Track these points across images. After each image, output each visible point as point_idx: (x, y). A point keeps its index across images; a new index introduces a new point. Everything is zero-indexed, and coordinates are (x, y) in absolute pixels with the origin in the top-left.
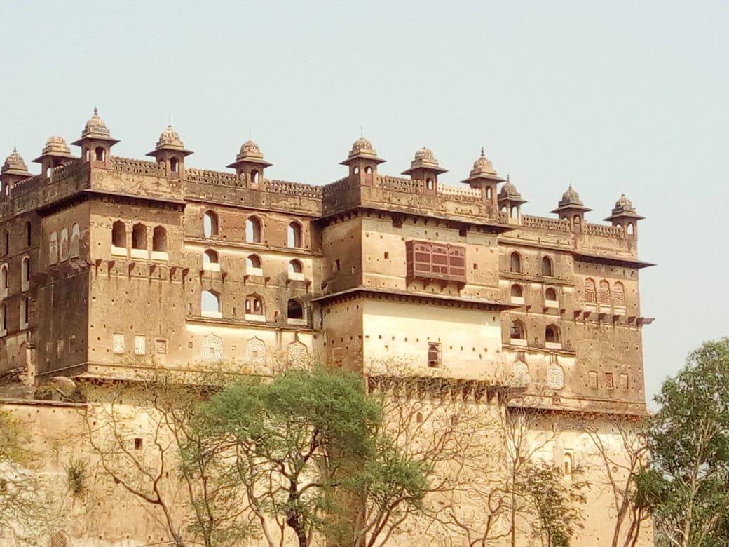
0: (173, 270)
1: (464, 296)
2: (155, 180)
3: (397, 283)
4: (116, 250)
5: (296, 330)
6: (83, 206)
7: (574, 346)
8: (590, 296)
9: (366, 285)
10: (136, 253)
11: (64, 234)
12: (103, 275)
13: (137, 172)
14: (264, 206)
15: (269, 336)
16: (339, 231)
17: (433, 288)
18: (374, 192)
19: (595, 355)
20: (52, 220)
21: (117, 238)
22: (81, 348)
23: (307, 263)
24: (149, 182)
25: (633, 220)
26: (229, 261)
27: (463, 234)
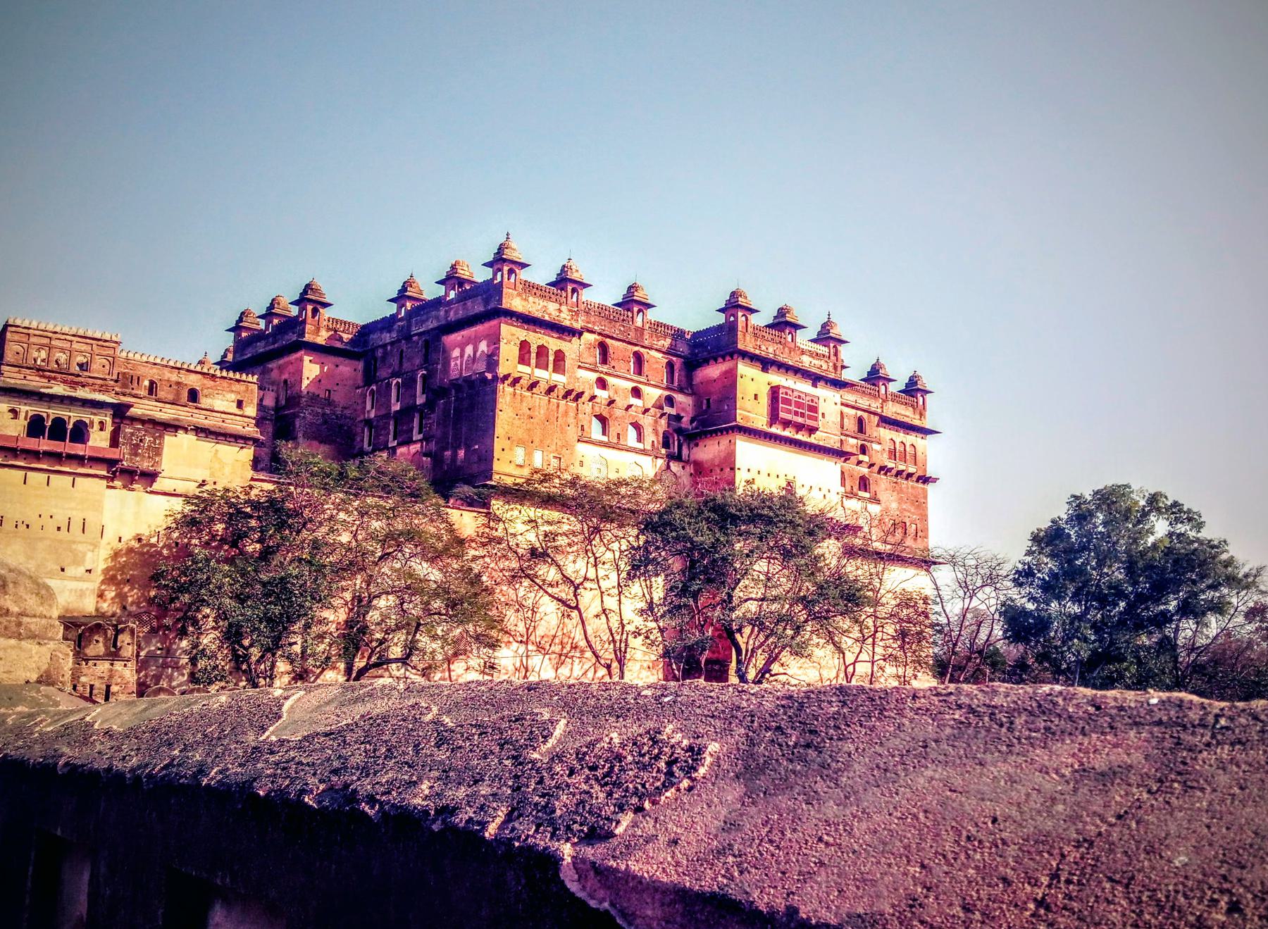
2: (557, 306)
4: (522, 368)
7: (880, 496)
9: (740, 421)
10: (540, 374)
11: (469, 350)
14: (646, 343)
16: (713, 371)
17: (791, 427)
18: (748, 338)
21: (523, 360)
22: (486, 459)
24: (552, 307)
27: (814, 385)
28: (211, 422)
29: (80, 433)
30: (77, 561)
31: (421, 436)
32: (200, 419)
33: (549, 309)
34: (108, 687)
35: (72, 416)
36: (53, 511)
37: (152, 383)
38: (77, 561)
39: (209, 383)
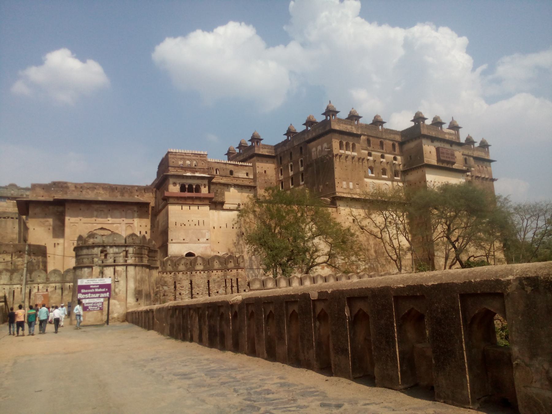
0: (359, 159)
1: (454, 167)
3: (434, 162)
5: (397, 181)
8: (479, 171)
10: (348, 153)
11: (319, 148)
12: (338, 160)
14: (384, 137)
15: (389, 183)
16: (412, 145)
17: (445, 165)
20: (313, 143)
23: (399, 158)
24: (349, 127)
26: (375, 156)
27: (451, 146)
28: (239, 182)
29: (198, 189)
30: (203, 236)
31: (303, 183)
34: (237, 279)
35: (194, 182)
36: (193, 218)
38: (203, 236)
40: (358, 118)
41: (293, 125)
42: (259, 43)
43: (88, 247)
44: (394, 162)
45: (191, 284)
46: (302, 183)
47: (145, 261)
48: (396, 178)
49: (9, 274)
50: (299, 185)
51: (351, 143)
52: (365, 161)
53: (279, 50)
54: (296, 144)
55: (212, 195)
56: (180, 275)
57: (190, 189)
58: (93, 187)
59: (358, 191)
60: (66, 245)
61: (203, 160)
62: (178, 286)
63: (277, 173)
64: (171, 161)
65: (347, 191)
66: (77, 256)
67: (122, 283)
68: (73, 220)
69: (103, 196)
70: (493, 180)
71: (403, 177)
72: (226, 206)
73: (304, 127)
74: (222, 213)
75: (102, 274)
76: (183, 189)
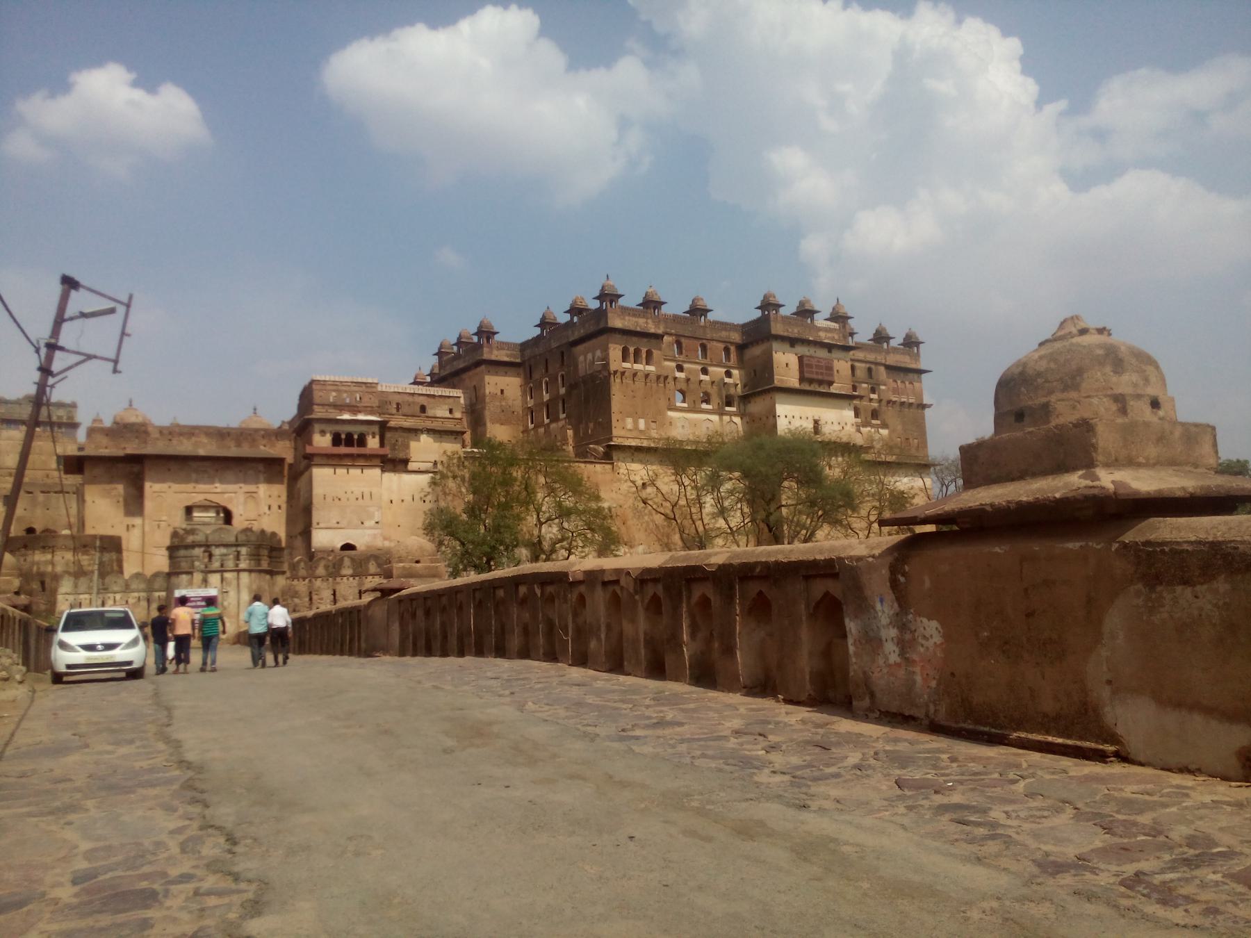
0: (658, 377)
3: (794, 382)
5: (730, 414)
6: (602, 339)
9: (777, 383)
10: (637, 367)
11: (590, 356)
12: (618, 380)
13: (634, 315)
14: (709, 336)
15: (715, 418)
16: (756, 351)
17: (815, 387)
19: (899, 428)
20: (580, 348)
21: (624, 359)
22: (607, 427)
23: (735, 372)
24: (641, 321)
25: (917, 344)
26: (690, 371)
27: (830, 351)
28: (436, 425)
29: (362, 442)
30: (371, 517)
32: (429, 424)
33: (641, 324)
35: (355, 430)
37: (398, 404)
38: (371, 517)
39: (432, 400)
40: (658, 304)
41: (552, 309)
42: (550, 55)
43: (187, 547)
44: (727, 380)
45: (334, 594)
46: (562, 416)
47: (265, 565)
48: (728, 409)
49: (72, 579)
50: (556, 419)
51: (644, 350)
52: (670, 379)
53: (598, 76)
54: (554, 345)
55: (387, 451)
56: (318, 583)
57: (349, 441)
58: (191, 432)
59: (654, 434)
60: (147, 528)
61: (371, 393)
62: (315, 597)
63: (524, 394)
64: (318, 395)
65: (634, 434)
66: (171, 557)
67: (232, 594)
68: (157, 487)
69: (206, 448)
70: (923, 406)
71: (742, 407)
72: (411, 466)
73: (567, 317)
74: (406, 477)
75: (205, 582)
76: (336, 440)
